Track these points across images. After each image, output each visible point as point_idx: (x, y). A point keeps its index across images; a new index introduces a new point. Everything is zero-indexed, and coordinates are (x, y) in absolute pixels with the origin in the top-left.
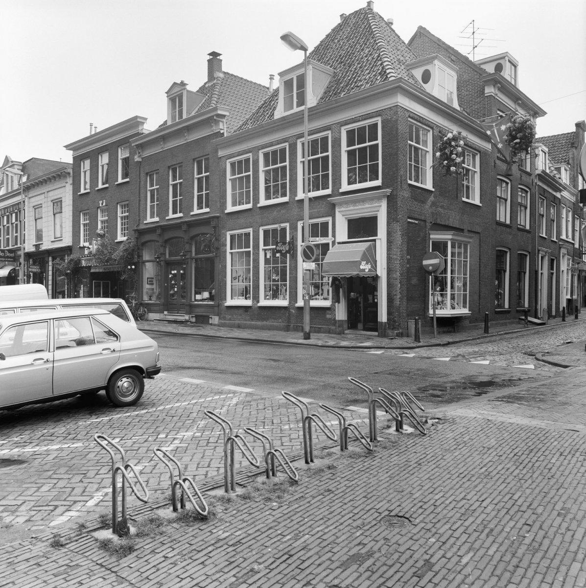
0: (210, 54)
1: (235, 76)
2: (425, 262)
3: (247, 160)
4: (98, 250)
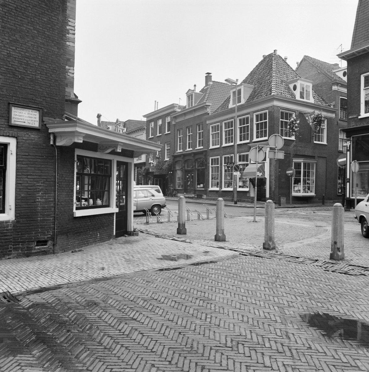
0: (206, 74)
1: (218, 82)
2: (288, 172)
3: (218, 126)
4: (157, 164)
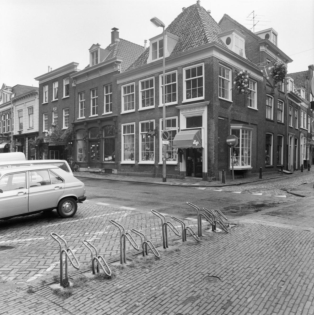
0: (112, 29)
1: (126, 41)
2: (228, 141)
3: (133, 86)
4: (52, 134)
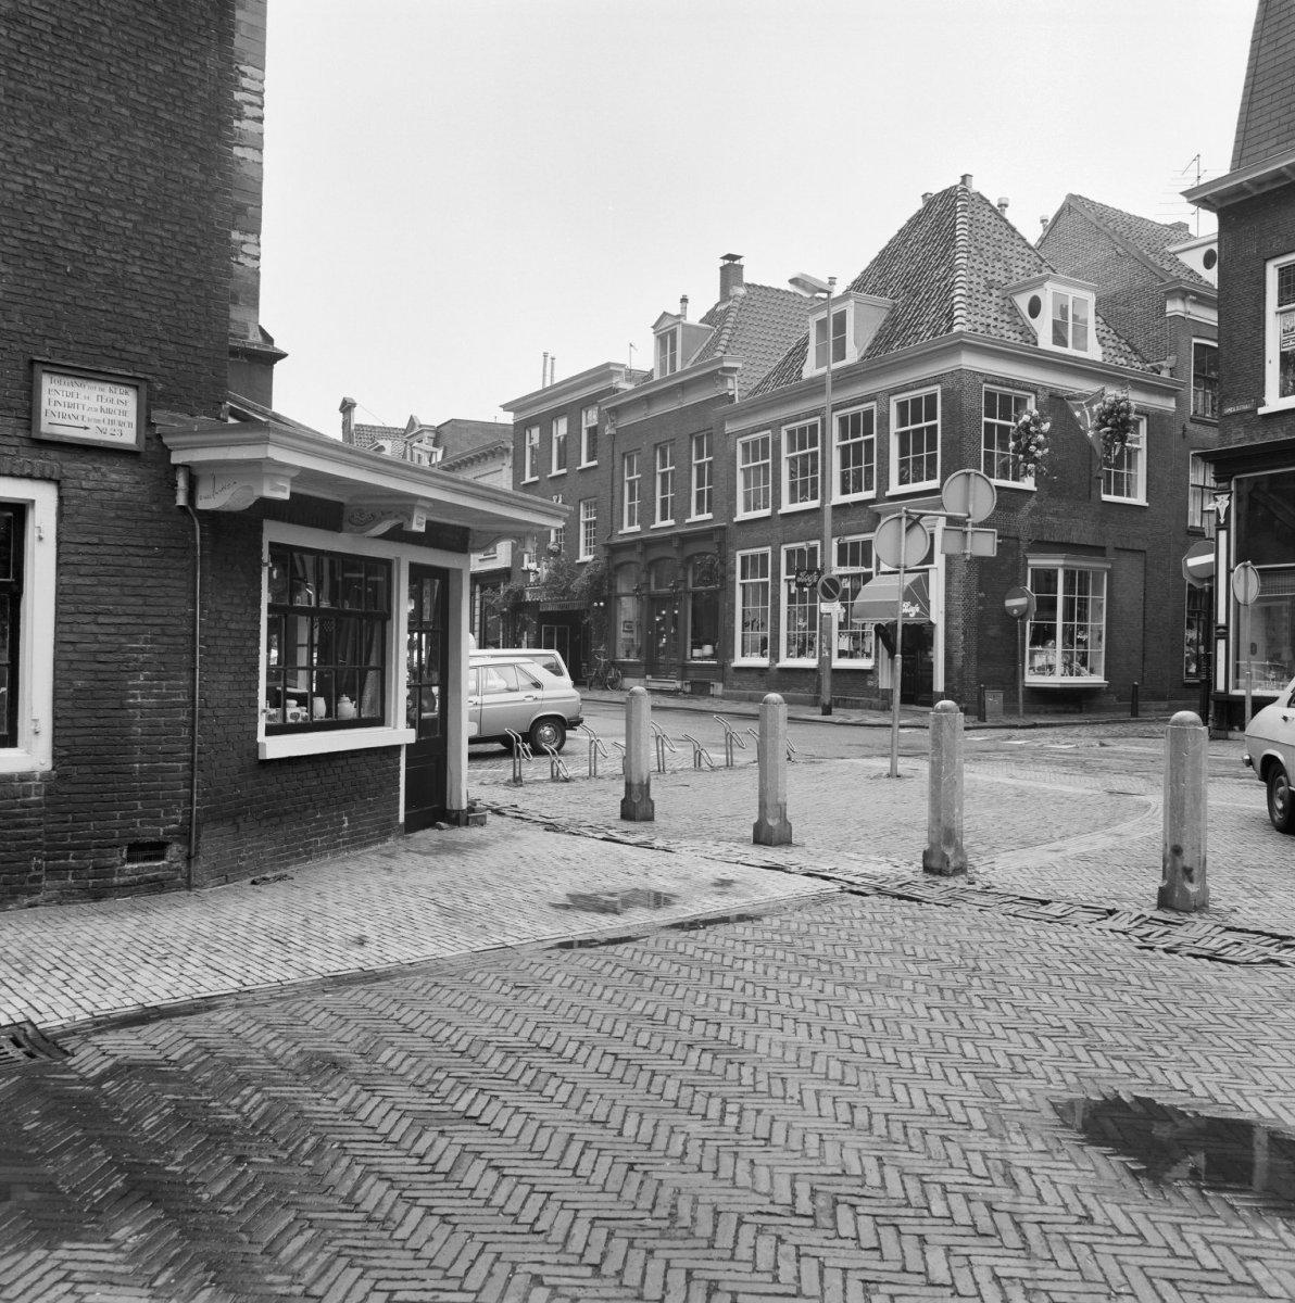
0: (724, 258)
1: (766, 288)
2: (1009, 603)
3: (765, 440)
4: (549, 576)
